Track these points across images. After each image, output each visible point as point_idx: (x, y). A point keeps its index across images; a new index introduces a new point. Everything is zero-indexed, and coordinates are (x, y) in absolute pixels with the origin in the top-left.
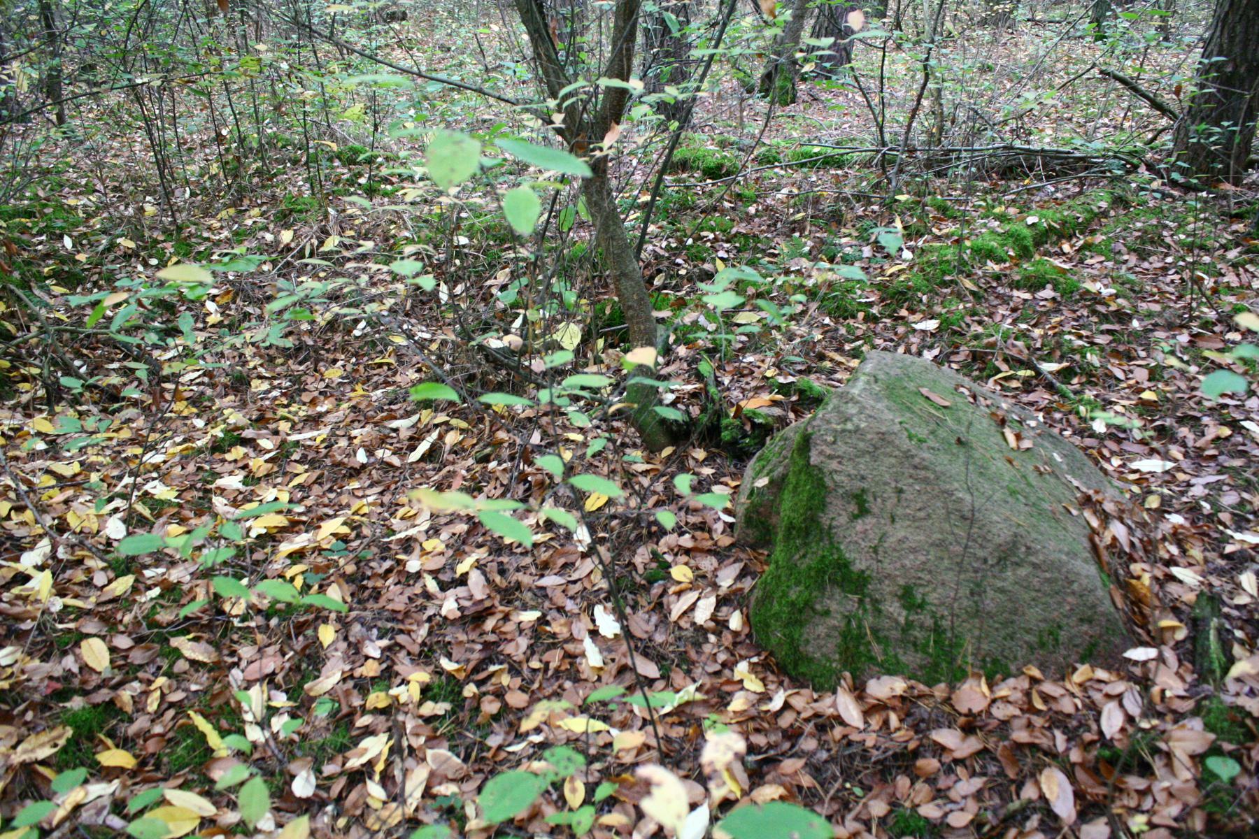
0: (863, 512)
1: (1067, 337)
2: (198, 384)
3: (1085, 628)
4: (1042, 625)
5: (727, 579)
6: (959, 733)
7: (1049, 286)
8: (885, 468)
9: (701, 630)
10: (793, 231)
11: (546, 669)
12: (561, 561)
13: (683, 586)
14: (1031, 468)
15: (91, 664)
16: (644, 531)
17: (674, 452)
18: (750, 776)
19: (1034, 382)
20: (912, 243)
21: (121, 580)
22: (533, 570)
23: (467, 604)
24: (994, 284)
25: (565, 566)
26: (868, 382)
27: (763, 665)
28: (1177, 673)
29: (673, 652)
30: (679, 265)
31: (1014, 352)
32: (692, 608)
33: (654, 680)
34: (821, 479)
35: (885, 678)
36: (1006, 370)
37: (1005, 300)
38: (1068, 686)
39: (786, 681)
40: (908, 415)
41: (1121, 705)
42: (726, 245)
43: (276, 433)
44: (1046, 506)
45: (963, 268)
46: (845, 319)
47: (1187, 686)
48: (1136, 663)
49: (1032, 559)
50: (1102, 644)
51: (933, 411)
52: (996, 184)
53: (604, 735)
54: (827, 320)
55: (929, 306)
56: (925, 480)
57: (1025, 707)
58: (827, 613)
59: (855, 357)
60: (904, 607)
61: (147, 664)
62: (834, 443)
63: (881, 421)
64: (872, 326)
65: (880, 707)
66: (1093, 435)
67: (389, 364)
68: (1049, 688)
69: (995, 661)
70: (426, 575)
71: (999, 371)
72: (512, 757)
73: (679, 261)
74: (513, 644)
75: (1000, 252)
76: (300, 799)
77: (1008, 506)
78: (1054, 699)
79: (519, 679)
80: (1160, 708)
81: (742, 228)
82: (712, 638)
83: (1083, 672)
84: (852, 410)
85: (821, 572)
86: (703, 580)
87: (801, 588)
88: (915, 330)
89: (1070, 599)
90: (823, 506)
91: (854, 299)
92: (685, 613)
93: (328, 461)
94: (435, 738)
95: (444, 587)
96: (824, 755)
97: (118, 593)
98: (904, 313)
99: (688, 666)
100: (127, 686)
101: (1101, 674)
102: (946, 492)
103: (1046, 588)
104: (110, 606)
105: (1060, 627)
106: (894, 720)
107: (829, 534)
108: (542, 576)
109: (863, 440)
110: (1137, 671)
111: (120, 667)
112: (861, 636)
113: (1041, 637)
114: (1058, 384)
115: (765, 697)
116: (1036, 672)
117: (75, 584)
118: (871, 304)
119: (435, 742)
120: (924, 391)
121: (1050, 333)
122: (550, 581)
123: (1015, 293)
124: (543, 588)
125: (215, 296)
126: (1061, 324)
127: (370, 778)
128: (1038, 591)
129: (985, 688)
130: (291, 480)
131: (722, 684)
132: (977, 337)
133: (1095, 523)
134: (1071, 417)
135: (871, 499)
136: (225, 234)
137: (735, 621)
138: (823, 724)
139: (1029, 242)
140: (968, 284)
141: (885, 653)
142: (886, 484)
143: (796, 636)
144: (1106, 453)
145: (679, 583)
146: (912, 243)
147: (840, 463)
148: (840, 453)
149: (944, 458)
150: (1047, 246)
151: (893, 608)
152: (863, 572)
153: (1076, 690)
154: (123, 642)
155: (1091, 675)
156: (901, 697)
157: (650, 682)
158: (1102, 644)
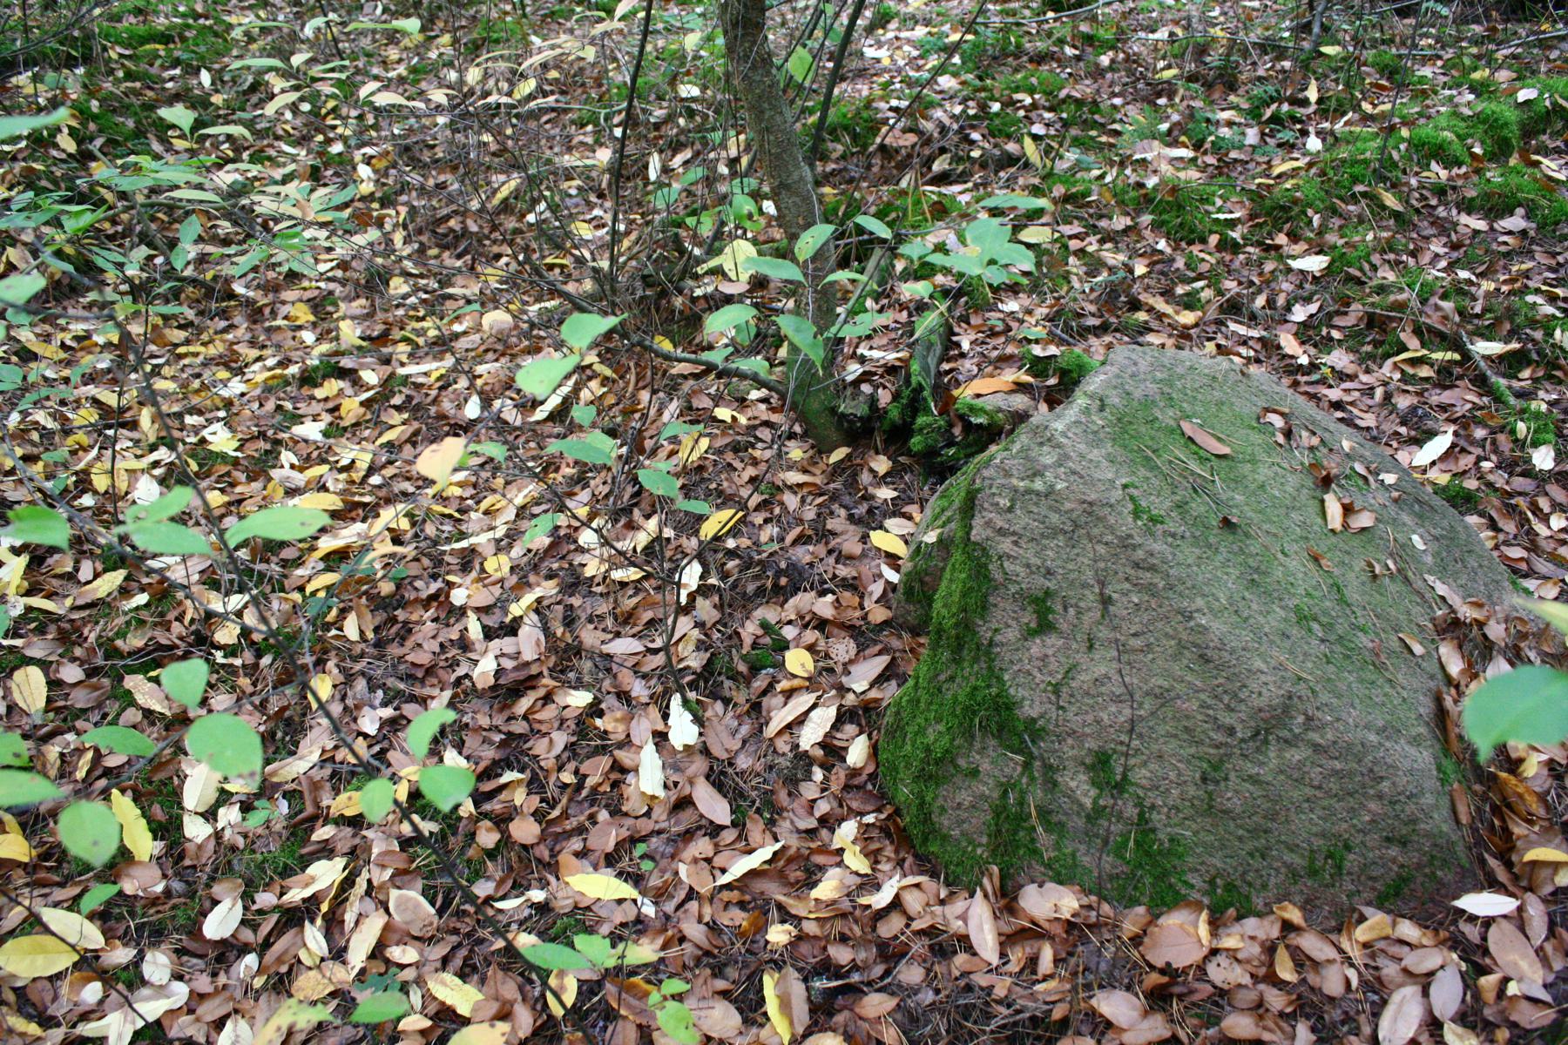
0: (1044, 626)
1: (1530, 299)
2: (330, 280)
3: (1393, 852)
4: (1318, 842)
5: (860, 680)
6: (1139, 1003)
7: (1520, 211)
8: (1084, 562)
9: (803, 760)
10: (1159, 95)
11: (579, 786)
12: (647, 615)
13: (796, 683)
14: (1360, 564)
15: (22, 704)
16: (769, 584)
17: (849, 456)
18: (813, 1011)
19: (1457, 371)
20: (1326, 125)
21: (109, 576)
22: (609, 622)
23: (508, 664)
24: (1434, 202)
25: (651, 623)
26: (1086, 411)
27: (881, 829)
28: (1540, 951)
29: (754, 788)
30: (972, 142)
31: (1433, 320)
32: (801, 720)
33: (723, 827)
34: (985, 566)
35: (1049, 885)
36: (1415, 348)
37: (1444, 228)
38: (1346, 945)
39: (910, 860)
40: (1143, 472)
41: (1425, 993)
42: (1048, 115)
43: (387, 361)
44: (1364, 640)
45: (1385, 172)
46: (1190, 243)
47: (1550, 978)
48: (1472, 919)
49: (1315, 736)
50: (1420, 879)
51: (1194, 466)
52: (1494, 30)
53: (628, 905)
54: (1162, 245)
55: (1320, 233)
56: (1150, 589)
57: (1262, 971)
58: (974, 773)
59: (1189, 307)
60: (1093, 783)
61: (92, 708)
62: (1010, 510)
63: (1092, 483)
64: (1228, 258)
65: (1034, 932)
66: (1529, 472)
67: (562, 266)
68: (1312, 944)
69: (1230, 887)
70: (470, 613)
71: (1405, 349)
72: (500, 917)
73: (975, 136)
74: (546, 740)
75: (1457, 149)
76: (209, 941)
77: (1287, 644)
78: (1316, 965)
79: (537, 798)
80: (1488, 1013)
81: (1084, 89)
82: (818, 774)
83: (1375, 923)
84: (1048, 457)
85: (970, 712)
86: (826, 676)
87: (941, 727)
88: (1289, 270)
89: (1373, 806)
90: (984, 608)
91: (1208, 213)
92: (789, 726)
93: (433, 410)
94: (405, 872)
95: (489, 634)
96: (928, 997)
97: (101, 594)
98: (1281, 239)
99: (772, 813)
100: (59, 739)
101: (1408, 930)
102: (1181, 612)
103: (1333, 785)
104: (87, 612)
105: (1348, 848)
106: (1047, 955)
107: (988, 653)
108: (618, 635)
109: (1057, 511)
110: (1472, 932)
111: (58, 710)
112: (1022, 817)
113: (1312, 860)
114: (1494, 379)
115: (870, 883)
116: (1295, 915)
117: (56, 576)
118: (1232, 224)
119: (407, 878)
120: (1187, 427)
121: (1505, 288)
122: (624, 646)
123: (1464, 219)
124: (609, 657)
125: (372, 157)
126: (1526, 275)
127: (312, 921)
128: (1319, 787)
129: (1203, 930)
130: (380, 434)
131: (813, 851)
132: (1382, 289)
133: (1455, 667)
134: (1501, 438)
135: (1059, 608)
136: (402, 70)
137: (857, 752)
138: (945, 944)
139: (1513, 133)
140: (1390, 200)
141: (1057, 846)
142: (1085, 586)
143: (928, 799)
144: (1544, 504)
145: (795, 676)
146: (1326, 125)
147: (1016, 543)
148: (1017, 528)
149: (1189, 553)
150: (1544, 138)
151: (1080, 787)
152: (1034, 721)
153: (1356, 954)
154: (71, 673)
155: (1389, 931)
156: (1068, 921)
157: (714, 830)
158: (1420, 879)
